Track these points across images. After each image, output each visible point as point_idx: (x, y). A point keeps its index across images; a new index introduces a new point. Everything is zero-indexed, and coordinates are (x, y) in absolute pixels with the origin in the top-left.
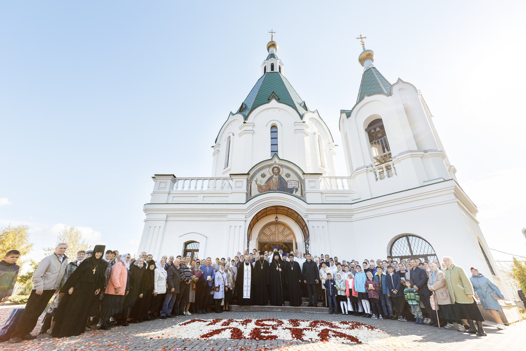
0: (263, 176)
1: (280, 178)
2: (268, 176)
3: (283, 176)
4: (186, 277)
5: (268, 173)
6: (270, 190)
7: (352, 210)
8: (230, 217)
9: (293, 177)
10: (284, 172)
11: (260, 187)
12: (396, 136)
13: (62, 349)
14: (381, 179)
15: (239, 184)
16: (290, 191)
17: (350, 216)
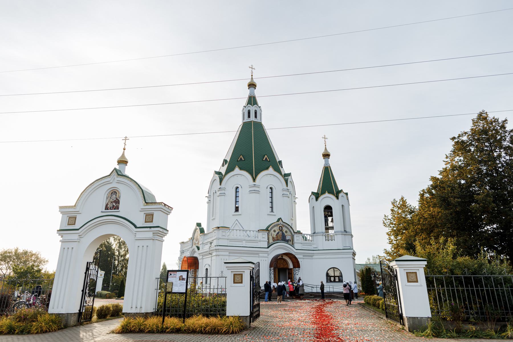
0: (275, 231)
1: (283, 233)
2: (277, 232)
3: (284, 232)
4: (34, 304)
5: (277, 229)
6: (278, 240)
7: (313, 254)
8: (261, 255)
9: (289, 233)
10: (285, 229)
11: (273, 238)
12: (336, 221)
13: (500, 170)
14: (332, 240)
15: (264, 236)
16: (287, 241)
17: (312, 256)
